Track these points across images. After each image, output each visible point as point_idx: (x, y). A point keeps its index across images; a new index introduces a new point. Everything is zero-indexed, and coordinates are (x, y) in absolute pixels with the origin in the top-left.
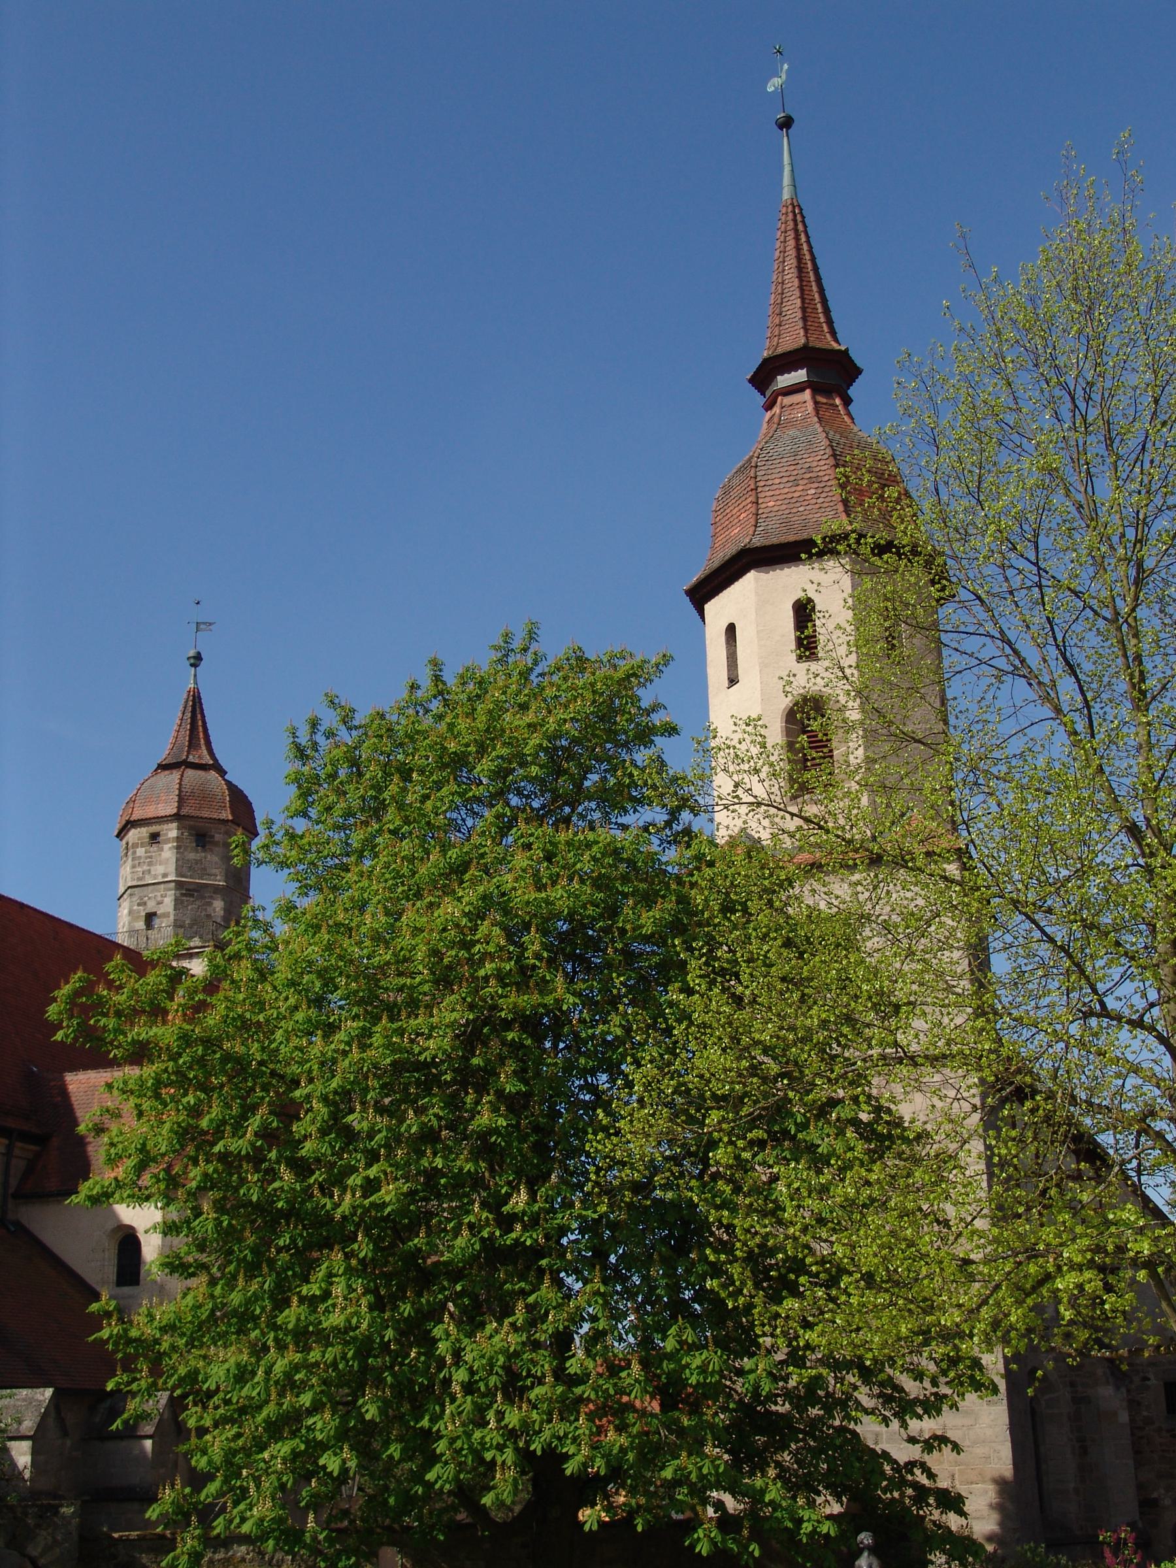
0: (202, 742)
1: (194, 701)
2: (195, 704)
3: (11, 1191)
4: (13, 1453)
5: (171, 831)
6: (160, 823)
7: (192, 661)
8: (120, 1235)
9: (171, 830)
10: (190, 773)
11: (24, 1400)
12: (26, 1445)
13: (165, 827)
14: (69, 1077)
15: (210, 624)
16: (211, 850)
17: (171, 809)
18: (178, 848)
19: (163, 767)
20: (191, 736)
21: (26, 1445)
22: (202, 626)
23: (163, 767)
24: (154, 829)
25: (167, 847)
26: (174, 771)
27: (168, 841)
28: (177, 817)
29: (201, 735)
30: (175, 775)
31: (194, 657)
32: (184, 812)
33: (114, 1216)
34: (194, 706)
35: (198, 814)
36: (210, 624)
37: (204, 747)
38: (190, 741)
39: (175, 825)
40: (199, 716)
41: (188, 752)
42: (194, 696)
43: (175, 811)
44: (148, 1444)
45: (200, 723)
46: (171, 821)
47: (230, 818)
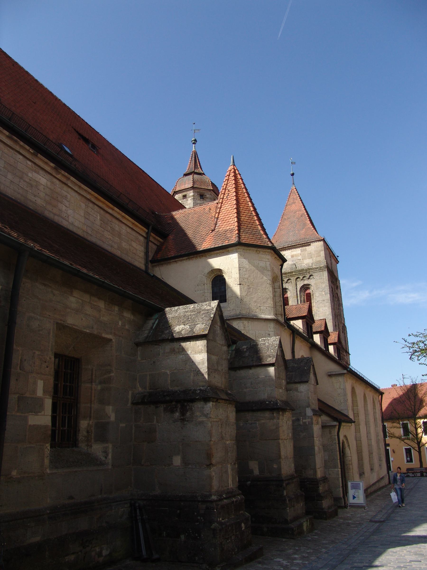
0: (199, 167)
1: (195, 154)
2: (196, 155)
3: (150, 259)
4: (189, 352)
5: (191, 193)
6: (186, 191)
7: (193, 142)
8: (213, 276)
9: (190, 193)
10: (196, 176)
11: (192, 311)
12: (201, 344)
13: (188, 192)
14: (174, 213)
15: (199, 130)
16: (206, 200)
17: (191, 185)
18: (194, 199)
19: (186, 175)
20: (195, 165)
21: (201, 344)
22: (196, 131)
23: (186, 175)
24: (184, 194)
25: (189, 199)
26: (190, 176)
27: (190, 197)
28: (193, 188)
29: (198, 165)
30: (191, 176)
31: (194, 140)
32: (195, 186)
33: (209, 265)
34: (195, 156)
35: (200, 187)
36: (199, 130)
37: (200, 168)
38: (195, 166)
39: (192, 191)
40: (197, 159)
41: (195, 170)
42: (195, 153)
43: (192, 185)
44: (272, 370)
45: (198, 161)
46: (190, 190)
47: (212, 189)
